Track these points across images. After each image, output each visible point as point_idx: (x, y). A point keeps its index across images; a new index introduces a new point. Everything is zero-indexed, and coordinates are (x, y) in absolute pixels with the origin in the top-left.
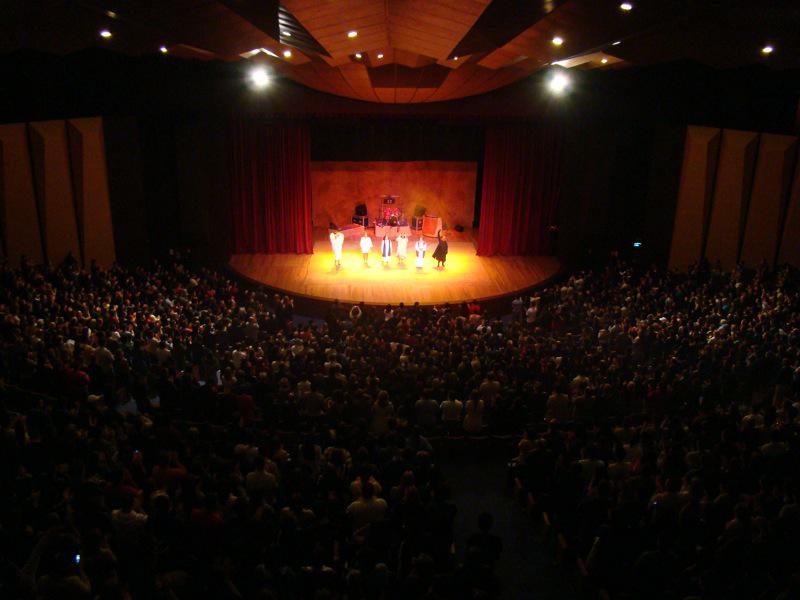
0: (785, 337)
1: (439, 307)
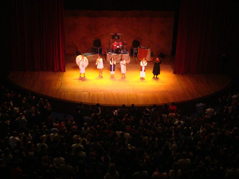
0: (180, 120)
1: (150, 107)
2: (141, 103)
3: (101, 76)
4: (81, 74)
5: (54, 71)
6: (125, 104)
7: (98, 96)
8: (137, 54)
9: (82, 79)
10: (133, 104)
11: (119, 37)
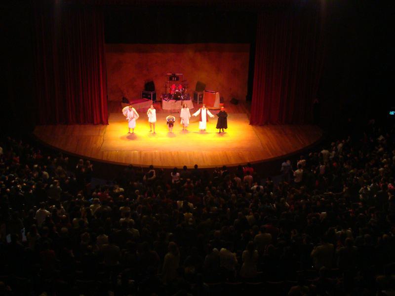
2: (208, 164)
3: (153, 132)
4: (129, 129)
5: (94, 124)
6: (187, 166)
7: (152, 155)
8: (202, 100)
9: (132, 137)
10: (185, 165)
11: (178, 78)
